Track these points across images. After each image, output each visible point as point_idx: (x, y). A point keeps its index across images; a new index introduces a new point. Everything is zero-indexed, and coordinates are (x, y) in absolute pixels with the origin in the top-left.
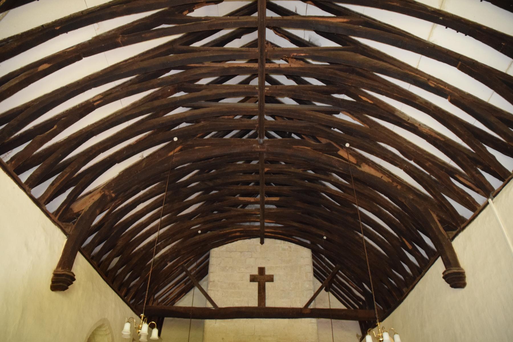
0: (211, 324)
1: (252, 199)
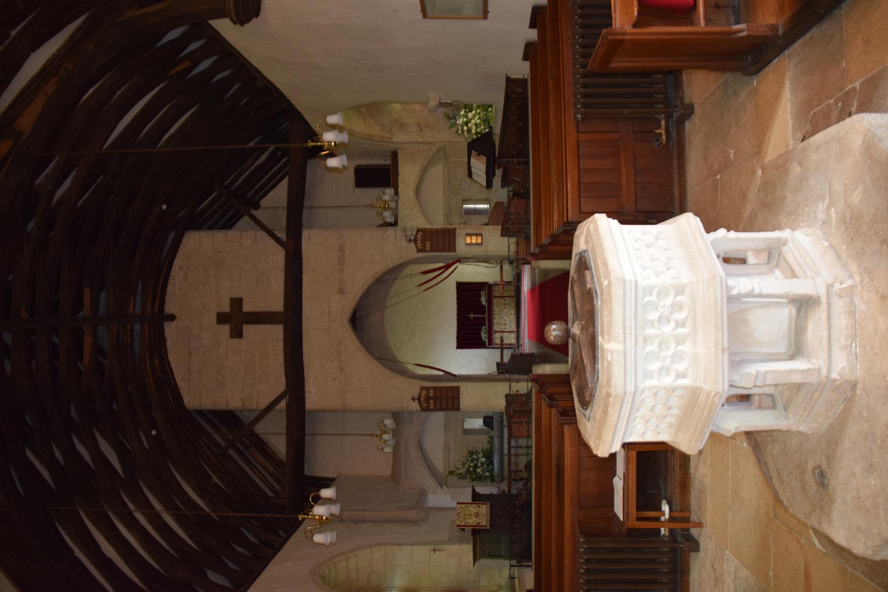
0: (313, 400)
1: (88, 340)
